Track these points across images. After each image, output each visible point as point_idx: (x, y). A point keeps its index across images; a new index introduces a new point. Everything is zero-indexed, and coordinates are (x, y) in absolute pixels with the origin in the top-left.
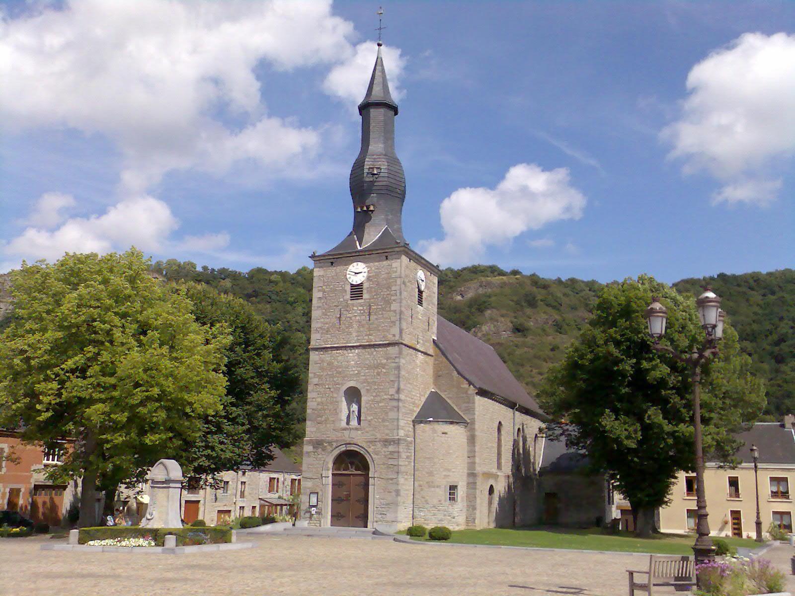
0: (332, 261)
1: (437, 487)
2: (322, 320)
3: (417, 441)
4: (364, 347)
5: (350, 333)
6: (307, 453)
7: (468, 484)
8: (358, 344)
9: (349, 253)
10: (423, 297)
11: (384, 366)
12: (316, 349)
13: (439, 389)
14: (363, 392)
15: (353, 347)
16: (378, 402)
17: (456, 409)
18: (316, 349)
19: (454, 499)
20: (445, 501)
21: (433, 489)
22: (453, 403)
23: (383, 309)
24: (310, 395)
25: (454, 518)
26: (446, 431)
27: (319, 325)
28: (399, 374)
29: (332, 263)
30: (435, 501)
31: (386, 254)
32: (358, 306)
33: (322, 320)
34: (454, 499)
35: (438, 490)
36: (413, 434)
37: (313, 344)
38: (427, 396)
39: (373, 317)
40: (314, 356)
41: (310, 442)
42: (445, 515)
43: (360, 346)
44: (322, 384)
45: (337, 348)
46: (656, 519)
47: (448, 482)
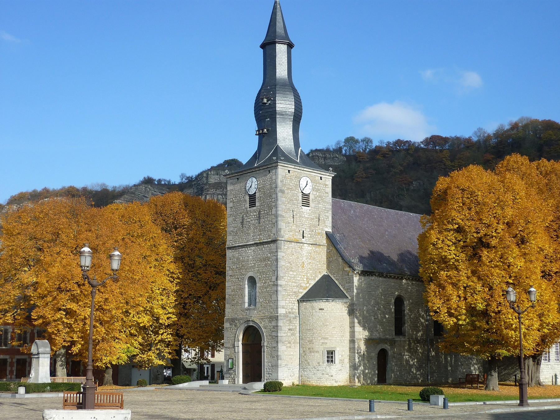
0: (237, 177)
1: (316, 352)
2: (233, 225)
3: (302, 316)
4: (257, 244)
5: (249, 234)
6: (227, 328)
7: (350, 348)
8: (253, 243)
9: (241, 172)
10: (310, 199)
11: (268, 259)
12: (230, 248)
13: (331, 273)
14: (257, 280)
15: (250, 245)
16: (266, 288)
17: (342, 289)
18: (230, 248)
19: (332, 361)
20: (323, 363)
21: (313, 354)
22: (340, 284)
23: (267, 214)
24: (227, 284)
25: (332, 376)
26: (322, 307)
27: (232, 229)
28: (277, 265)
29: (238, 179)
30: (315, 364)
31: (237, 177)
32: (253, 212)
33: (233, 225)
34: (332, 361)
35: (317, 354)
36: (297, 311)
37: (229, 244)
38: (317, 279)
39: (262, 220)
40: (229, 253)
41: (228, 320)
42: (323, 374)
43: (255, 244)
44: (234, 275)
45: (242, 247)
46: (27, 369)
47: (326, 348)
